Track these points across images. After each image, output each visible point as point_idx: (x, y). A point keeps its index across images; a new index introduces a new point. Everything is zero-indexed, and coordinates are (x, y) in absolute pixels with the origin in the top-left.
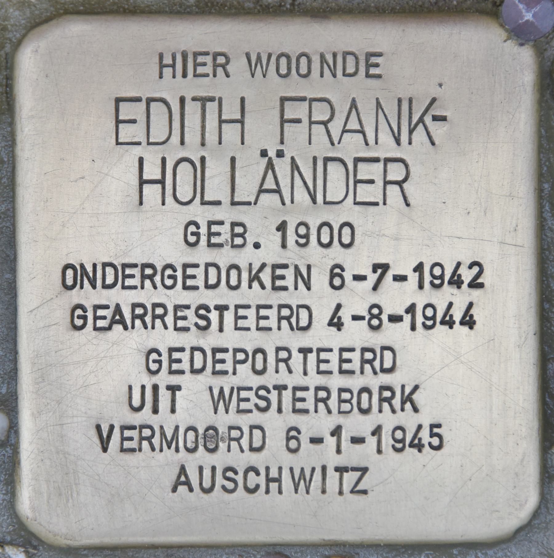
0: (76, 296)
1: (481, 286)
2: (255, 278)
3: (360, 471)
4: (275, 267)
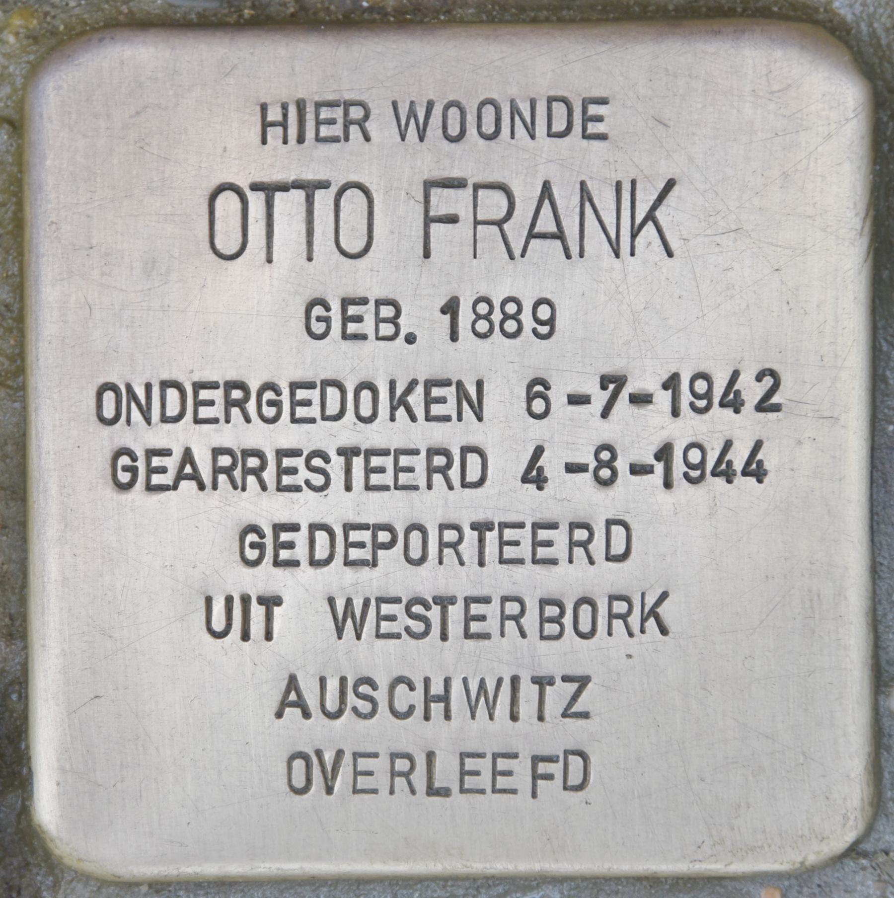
0: (121, 435)
1: (777, 408)
2: (399, 402)
3: (578, 682)
4: (430, 384)
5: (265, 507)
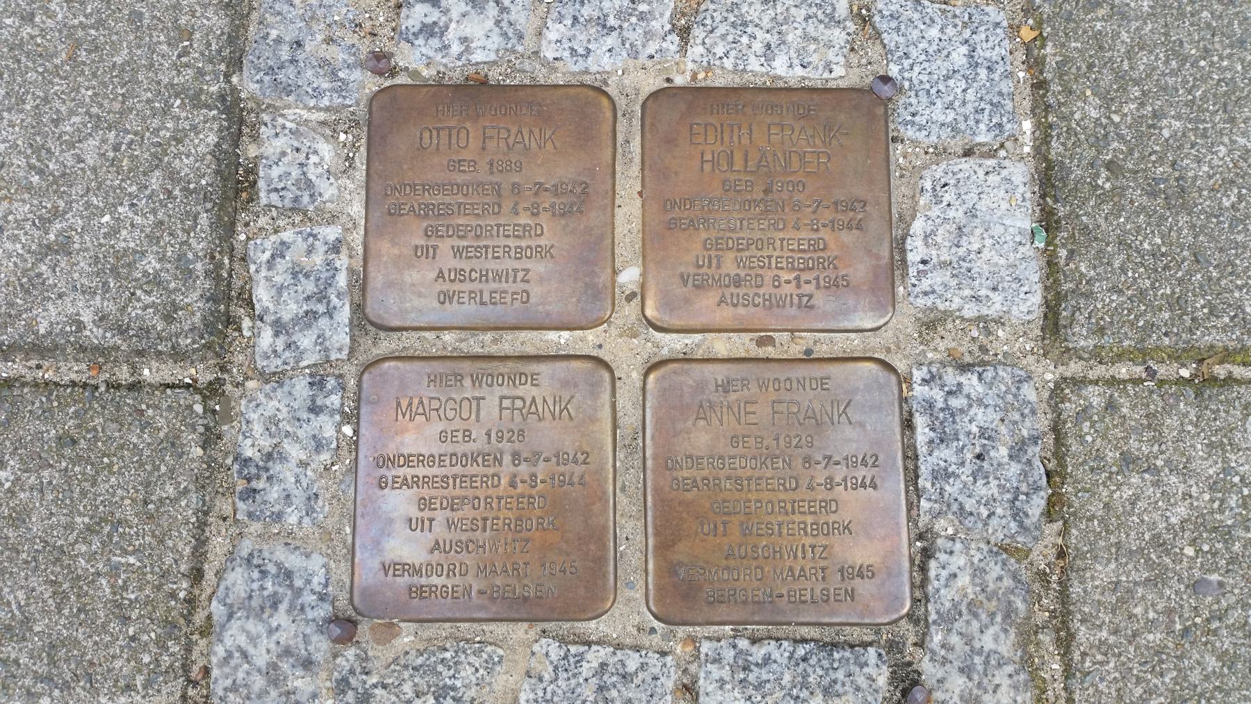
0: (383, 471)
5: (426, 492)
